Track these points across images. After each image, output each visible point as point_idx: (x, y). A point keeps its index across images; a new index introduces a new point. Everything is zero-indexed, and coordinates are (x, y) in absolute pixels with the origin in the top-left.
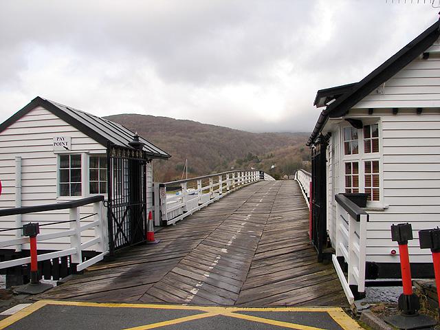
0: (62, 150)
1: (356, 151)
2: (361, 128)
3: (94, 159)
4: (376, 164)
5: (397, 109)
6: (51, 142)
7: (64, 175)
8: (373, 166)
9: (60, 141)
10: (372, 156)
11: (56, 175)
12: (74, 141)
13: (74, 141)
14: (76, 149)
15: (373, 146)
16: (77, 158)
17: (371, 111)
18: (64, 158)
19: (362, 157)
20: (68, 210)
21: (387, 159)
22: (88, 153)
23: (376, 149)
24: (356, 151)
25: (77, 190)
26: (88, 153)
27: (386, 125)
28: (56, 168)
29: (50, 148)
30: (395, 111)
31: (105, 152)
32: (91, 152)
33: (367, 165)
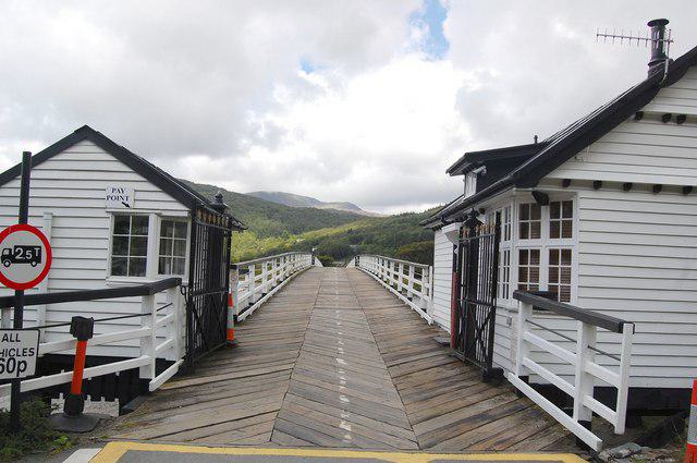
0: (118, 207)
1: (537, 235)
2: (546, 203)
3: (167, 224)
4: (567, 254)
5: (631, 184)
6: (103, 195)
7: (119, 245)
8: (561, 257)
9: (116, 194)
10: (561, 243)
11: (108, 244)
12: (140, 196)
13: (140, 196)
14: (139, 207)
15: (562, 229)
16: (142, 221)
17: (567, 183)
18: (121, 222)
19: (545, 243)
20: (140, 298)
21: (585, 248)
22: (159, 215)
23: (568, 233)
24: (537, 235)
25: (139, 268)
26: (159, 215)
27: (585, 203)
28: (109, 234)
29: (101, 204)
30: (597, 185)
31: (186, 214)
32: (165, 213)
33: (553, 255)
